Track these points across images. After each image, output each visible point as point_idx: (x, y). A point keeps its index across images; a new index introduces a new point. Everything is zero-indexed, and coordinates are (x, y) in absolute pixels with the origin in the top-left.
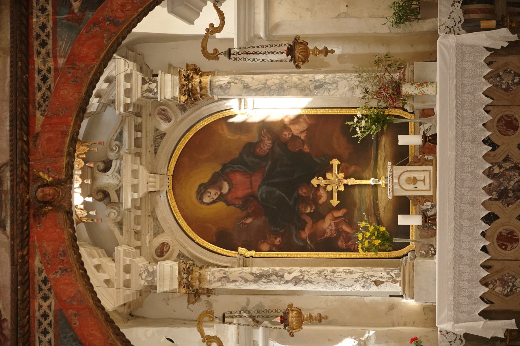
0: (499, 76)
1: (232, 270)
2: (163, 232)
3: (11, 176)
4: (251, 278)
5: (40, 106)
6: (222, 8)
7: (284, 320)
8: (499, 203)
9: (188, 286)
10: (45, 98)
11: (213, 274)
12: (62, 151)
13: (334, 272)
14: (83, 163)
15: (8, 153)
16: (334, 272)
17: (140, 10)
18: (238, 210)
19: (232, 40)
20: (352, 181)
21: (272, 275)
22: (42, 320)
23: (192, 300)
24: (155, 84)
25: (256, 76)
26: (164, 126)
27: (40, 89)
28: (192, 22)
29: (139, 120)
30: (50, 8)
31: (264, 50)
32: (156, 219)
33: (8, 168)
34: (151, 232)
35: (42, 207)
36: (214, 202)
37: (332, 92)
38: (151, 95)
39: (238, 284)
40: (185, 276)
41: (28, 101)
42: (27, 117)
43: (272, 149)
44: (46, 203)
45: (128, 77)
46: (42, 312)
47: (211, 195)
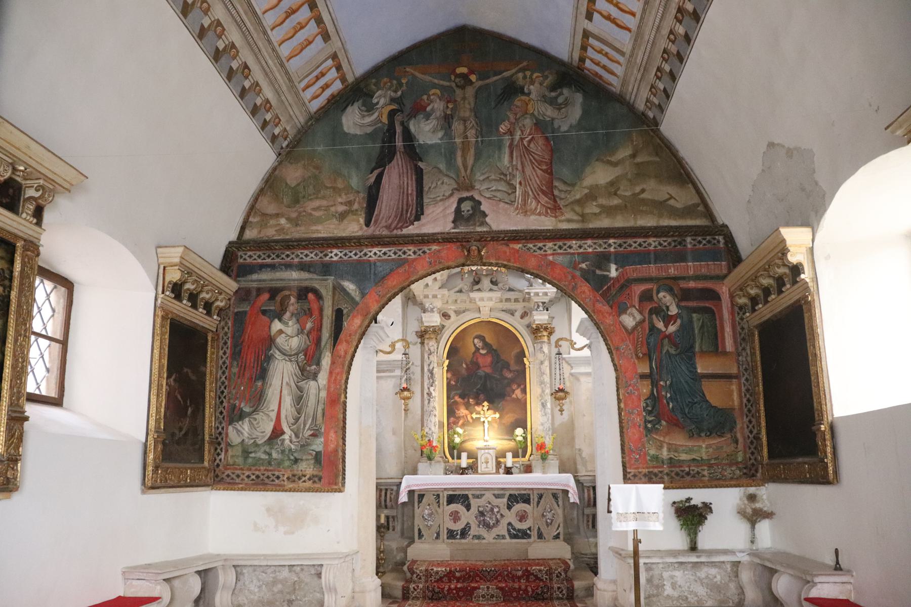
0: (551, 510)
1: (435, 357)
2: (457, 316)
3: (484, 231)
4: (431, 368)
5: (525, 246)
7: (405, 389)
11: (433, 346)
12: (498, 260)
15: (497, 229)
16: (435, 416)
17: (582, 303)
18: (470, 360)
22: (402, 251)
24: (542, 309)
27: (534, 246)
28: (577, 332)
29: (521, 300)
30: (581, 250)
31: (562, 379)
33: (488, 230)
34: (456, 309)
35: (466, 249)
36: (475, 345)
37: (540, 413)
38: (536, 307)
39: (427, 360)
40: (431, 330)
41: (527, 239)
42: (518, 239)
43: (506, 378)
44: (469, 251)
45: (546, 294)
46: (407, 251)
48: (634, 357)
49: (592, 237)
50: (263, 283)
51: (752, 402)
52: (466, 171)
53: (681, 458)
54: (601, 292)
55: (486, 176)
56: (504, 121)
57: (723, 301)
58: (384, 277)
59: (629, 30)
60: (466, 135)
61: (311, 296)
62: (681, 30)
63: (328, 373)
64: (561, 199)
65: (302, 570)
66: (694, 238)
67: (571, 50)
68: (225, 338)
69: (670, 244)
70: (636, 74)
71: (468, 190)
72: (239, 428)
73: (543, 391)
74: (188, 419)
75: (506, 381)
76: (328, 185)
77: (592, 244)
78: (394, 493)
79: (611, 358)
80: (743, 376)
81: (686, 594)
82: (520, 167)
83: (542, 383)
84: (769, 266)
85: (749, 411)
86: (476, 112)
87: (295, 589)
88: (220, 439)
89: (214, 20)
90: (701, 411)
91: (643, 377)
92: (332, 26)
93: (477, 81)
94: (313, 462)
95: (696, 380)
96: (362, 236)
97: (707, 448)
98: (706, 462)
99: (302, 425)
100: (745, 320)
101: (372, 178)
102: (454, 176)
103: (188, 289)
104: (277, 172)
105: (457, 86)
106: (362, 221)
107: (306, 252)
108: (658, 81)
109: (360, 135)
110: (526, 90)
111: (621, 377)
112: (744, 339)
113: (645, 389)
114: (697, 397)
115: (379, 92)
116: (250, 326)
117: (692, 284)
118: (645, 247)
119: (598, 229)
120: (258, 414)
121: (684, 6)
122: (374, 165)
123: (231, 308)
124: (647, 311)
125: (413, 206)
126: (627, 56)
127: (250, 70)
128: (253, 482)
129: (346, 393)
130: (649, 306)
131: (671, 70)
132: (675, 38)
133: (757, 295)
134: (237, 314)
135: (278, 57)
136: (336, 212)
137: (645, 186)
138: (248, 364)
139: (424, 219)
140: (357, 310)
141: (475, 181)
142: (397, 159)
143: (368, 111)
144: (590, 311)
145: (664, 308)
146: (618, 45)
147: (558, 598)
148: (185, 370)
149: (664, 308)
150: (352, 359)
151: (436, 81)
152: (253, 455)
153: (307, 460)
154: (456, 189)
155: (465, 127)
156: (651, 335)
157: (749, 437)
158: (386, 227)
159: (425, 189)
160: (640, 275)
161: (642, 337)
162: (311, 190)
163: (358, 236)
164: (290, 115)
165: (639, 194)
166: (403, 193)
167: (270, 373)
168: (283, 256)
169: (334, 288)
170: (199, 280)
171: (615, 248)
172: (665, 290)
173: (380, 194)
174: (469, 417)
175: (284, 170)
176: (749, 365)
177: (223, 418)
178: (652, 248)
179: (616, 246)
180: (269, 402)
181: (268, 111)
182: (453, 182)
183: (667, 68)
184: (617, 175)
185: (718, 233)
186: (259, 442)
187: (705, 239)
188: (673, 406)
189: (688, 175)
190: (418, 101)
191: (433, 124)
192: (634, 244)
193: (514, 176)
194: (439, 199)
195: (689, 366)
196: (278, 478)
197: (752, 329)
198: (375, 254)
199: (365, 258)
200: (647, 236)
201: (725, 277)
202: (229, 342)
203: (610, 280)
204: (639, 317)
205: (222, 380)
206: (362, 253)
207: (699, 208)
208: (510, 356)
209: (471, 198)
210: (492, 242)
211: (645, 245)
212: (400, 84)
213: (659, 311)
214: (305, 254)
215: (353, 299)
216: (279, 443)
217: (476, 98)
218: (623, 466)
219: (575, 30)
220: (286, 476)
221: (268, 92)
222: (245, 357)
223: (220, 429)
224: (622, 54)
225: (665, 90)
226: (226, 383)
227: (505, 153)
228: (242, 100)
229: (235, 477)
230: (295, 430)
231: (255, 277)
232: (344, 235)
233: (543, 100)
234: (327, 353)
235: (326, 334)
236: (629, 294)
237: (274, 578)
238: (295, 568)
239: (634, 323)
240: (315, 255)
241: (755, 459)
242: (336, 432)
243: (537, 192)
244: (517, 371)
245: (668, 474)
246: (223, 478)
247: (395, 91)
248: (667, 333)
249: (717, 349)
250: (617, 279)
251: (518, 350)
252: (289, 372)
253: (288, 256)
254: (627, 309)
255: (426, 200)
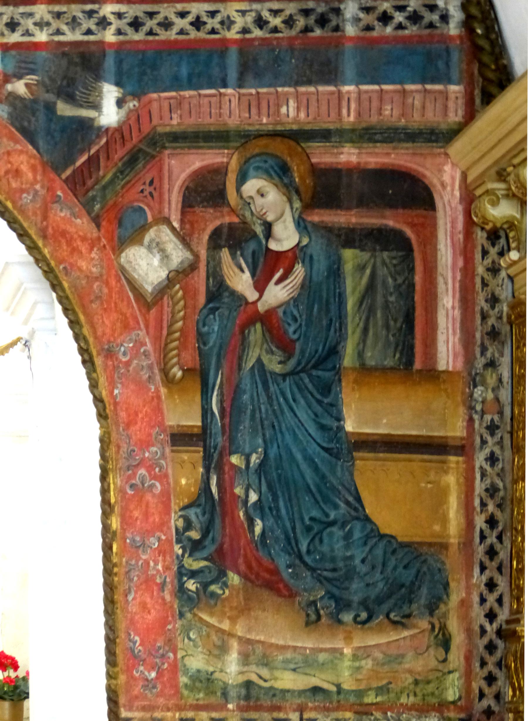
17: (9, 205)
30: (15, 38)
54: (69, 172)
57: (440, 213)
69: (289, 22)
77: (48, 17)
79: (89, 378)
80: (481, 448)
85: (491, 553)
90: (347, 547)
97: (355, 657)
98: (352, 699)
111: (114, 435)
114: (336, 507)
118: (213, 31)
124: (206, 237)
144: (32, 232)
145: (259, 230)
149: (259, 230)
156: (213, 311)
157: (483, 631)
161: (184, 318)
171: (119, 32)
172: (267, 172)
176: (501, 413)
178: (233, 34)
179: (123, 24)
188: (263, 533)
203: (99, 137)
211: (212, 23)
236: (151, 183)
239: (163, 274)
241: (498, 697)
248: (261, 307)
249: (410, 363)
254: (144, 228)
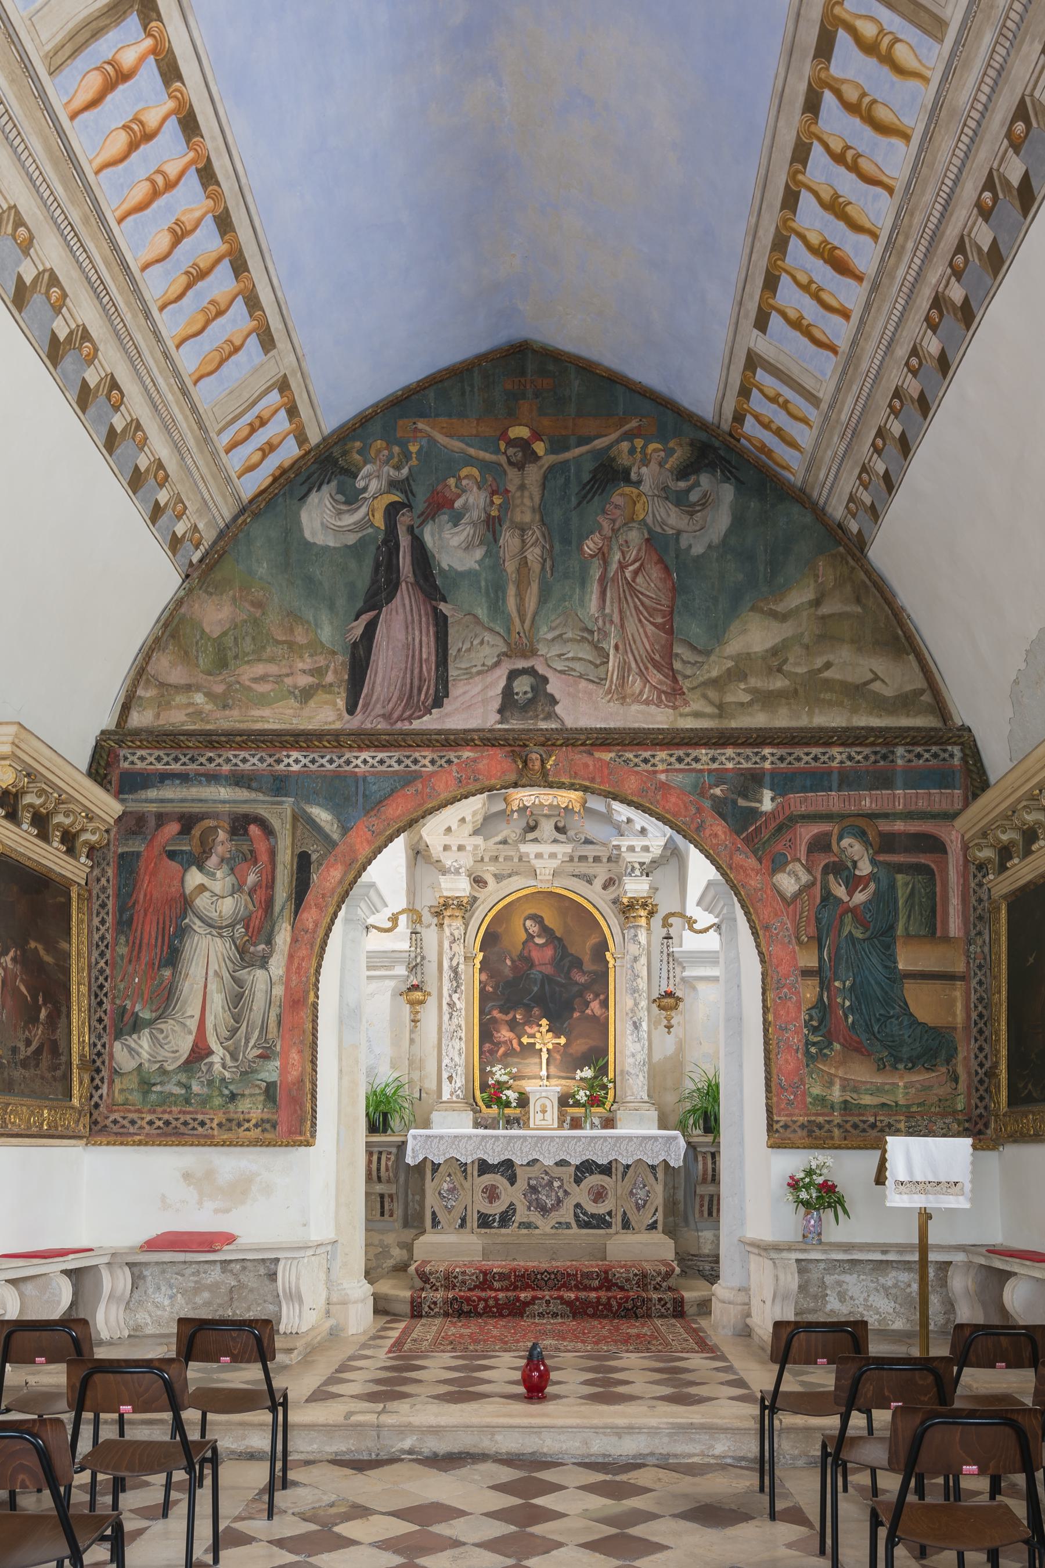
0: (645, 1186)
1: (462, 946)
4: (454, 963)
5: (620, 757)
6: (711, 931)
7: (415, 988)
8: (526, 1186)
9: (446, 905)
10: (627, 761)
12: (575, 778)
13: (460, 1039)
14: (563, 806)
15: (574, 726)
16: (460, 1039)
17: (711, 852)
19: (681, 946)
20: (545, 1056)
21: (457, 982)
22: (411, 759)
23: (433, 910)
25: (645, 968)
26: (598, 883)
27: (636, 756)
29: (605, 860)
30: (715, 766)
32: (510, 876)
33: (559, 727)
34: (497, 872)
35: (521, 758)
36: (526, 930)
38: (629, 870)
41: (625, 745)
42: (609, 744)
43: (577, 983)
44: (525, 763)
45: (646, 849)
46: (420, 758)
47: (533, 927)
48: (794, 940)
49: (735, 745)
50: (169, 805)
51: (983, 1020)
52: (523, 622)
53: (862, 1102)
54: (744, 835)
55: (557, 633)
56: (592, 533)
58: (381, 802)
59: (833, 349)
60: (526, 557)
61: (254, 830)
62: (933, 346)
63: (286, 956)
64: (686, 677)
65: (244, 1268)
66: (911, 748)
67: (720, 395)
68: (102, 896)
70: (836, 444)
71: (524, 655)
72: (133, 1045)
73: (636, 1004)
74: (41, 1027)
75: (575, 989)
76: (279, 638)
77: (733, 755)
78: (393, 1158)
81: (861, 1309)
82: (616, 618)
83: (635, 991)
84: (1041, 791)
85: (981, 1032)
86: (542, 512)
87: (231, 1299)
88: (98, 1063)
89: (44, 271)
91: (806, 973)
92: (278, 317)
93: (546, 454)
94: (262, 1098)
95: (894, 982)
96: (343, 730)
97: (905, 1087)
98: (904, 1109)
99: (243, 1041)
100: (985, 887)
101: (358, 628)
102: (502, 632)
103: (31, 805)
104: (183, 610)
105: (510, 463)
106: (341, 703)
107: (243, 754)
108: (875, 456)
109: (334, 548)
110: (633, 476)
112: (980, 918)
113: (809, 992)
114: (894, 1008)
115: (368, 468)
116: (147, 877)
117: (899, 826)
118: (824, 763)
119: (746, 729)
120: (166, 1022)
121: (947, 292)
122: (360, 604)
123: (111, 846)
125: (429, 681)
126: (824, 406)
127: (122, 395)
128: (159, 1131)
129: (318, 989)
130: (823, 860)
131: (903, 434)
132: (920, 364)
133: (1012, 843)
134: (122, 856)
135: (176, 373)
136: (295, 687)
137: (831, 657)
138: (145, 941)
139: (449, 705)
140: (335, 856)
141: (538, 641)
142: (403, 599)
143: (348, 502)
145: (849, 864)
146: (809, 384)
147: (662, 1316)
148: (33, 944)
149: (849, 864)
150: (327, 935)
151: (472, 451)
152: (158, 1088)
153: (251, 1095)
154: (505, 654)
155: (523, 541)
156: (824, 906)
157: (977, 1073)
158: (383, 716)
159: (450, 652)
160: (812, 809)
162: (248, 645)
163: (336, 730)
164: (203, 498)
165: (820, 671)
166: (413, 656)
167: (186, 954)
168: (203, 760)
169: (295, 818)
170: (51, 791)
171: (772, 763)
173: (372, 658)
174: (515, 1043)
175: (197, 606)
176: (985, 959)
177: (104, 1029)
178: (835, 764)
179: (774, 759)
180: (185, 1002)
181: (161, 486)
182: (500, 642)
183: (896, 428)
184: (784, 636)
185: (953, 740)
186: (170, 1068)
187: (928, 751)
188: (853, 1022)
189: (909, 638)
190: (440, 488)
191: (465, 533)
192: (805, 757)
193: (606, 635)
194: (474, 670)
195: (884, 957)
196: (202, 1124)
197: (995, 901)
198: (365, 762)
199: (347, 768)
200: (828, 744)
201: (955, 816)
202: (110, 904)
204: (805, 878)
205: (99, 966)
206: (343, 760)
207: (922, 698)
208: (583, 948)
209: (531, 672)
210: (564, 749)
211: (825, 758)
212: (406, 455)
213: (842, 869)
214: (241, 757)
215: (327, 837)
216: (204, 1068)
217: (544, 486)
218: (767, 1110)
219: (731, 353)
220: (216, 1122)
221: (160, 447)
222: (139, 928)
223: (99, 1047)
224: (813, 399)
225: (887, 476)
226: (108, 972)
227: (592, 592)
228: (111, 455)
229: (127, 1125)
230: (232, 1049)
231: (152, 793)
232: (310, 727)
233: (664, 495)
234: (284, 925)
235: (282, 893)
237: (196, 1282)
238: (233, 1265)
239: (797, 888)
240: (259, 760)
241: (986, 1108)
242: (300, 1052)
243: (644, 664)
244: (595, 973)
245: (839, 1126)
246: (106, 1126)
247: (398, 468)
248: (851, 905)
249: (934, 933)
250: (773, 814)
251: (597, 940)
252: (219, 955)
253: (210, 760)
254: (787, 863)
255: (452, 672)
